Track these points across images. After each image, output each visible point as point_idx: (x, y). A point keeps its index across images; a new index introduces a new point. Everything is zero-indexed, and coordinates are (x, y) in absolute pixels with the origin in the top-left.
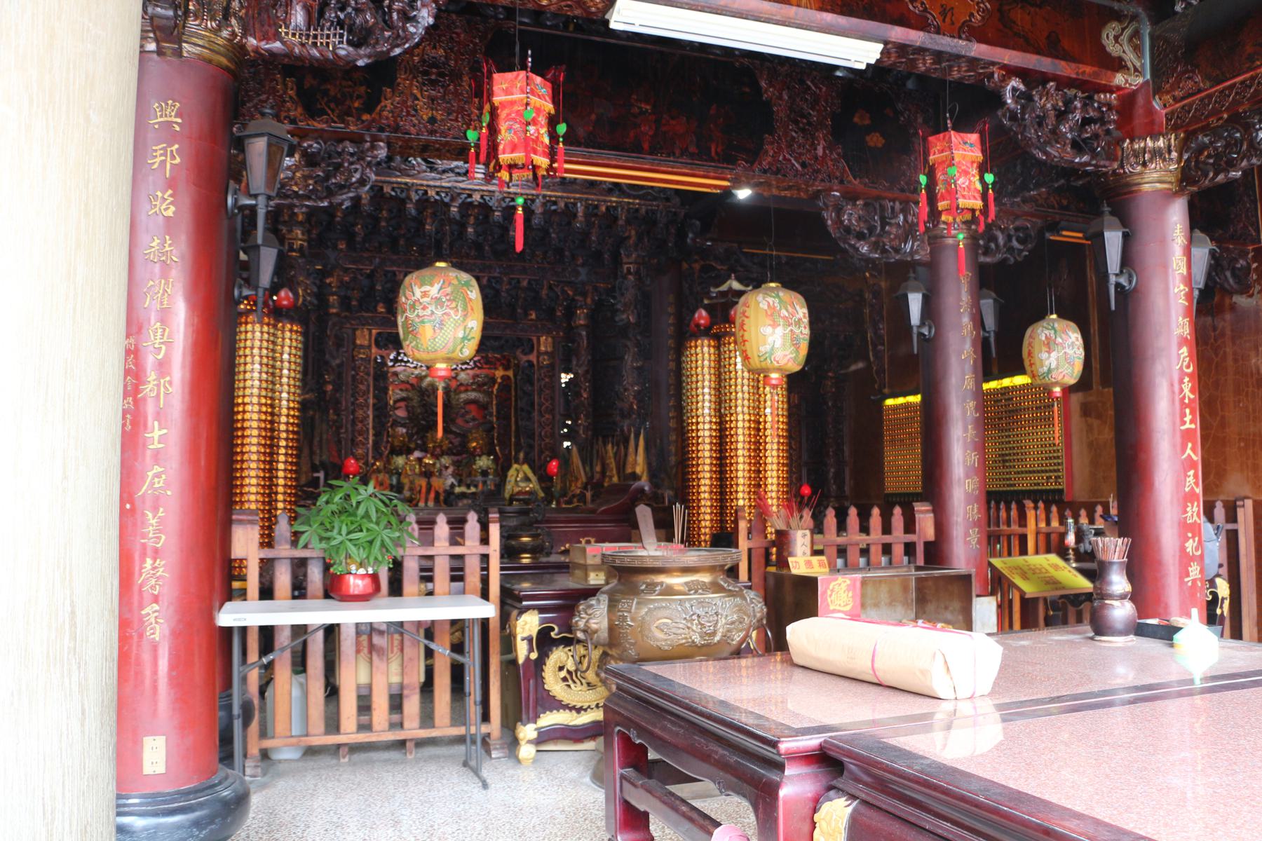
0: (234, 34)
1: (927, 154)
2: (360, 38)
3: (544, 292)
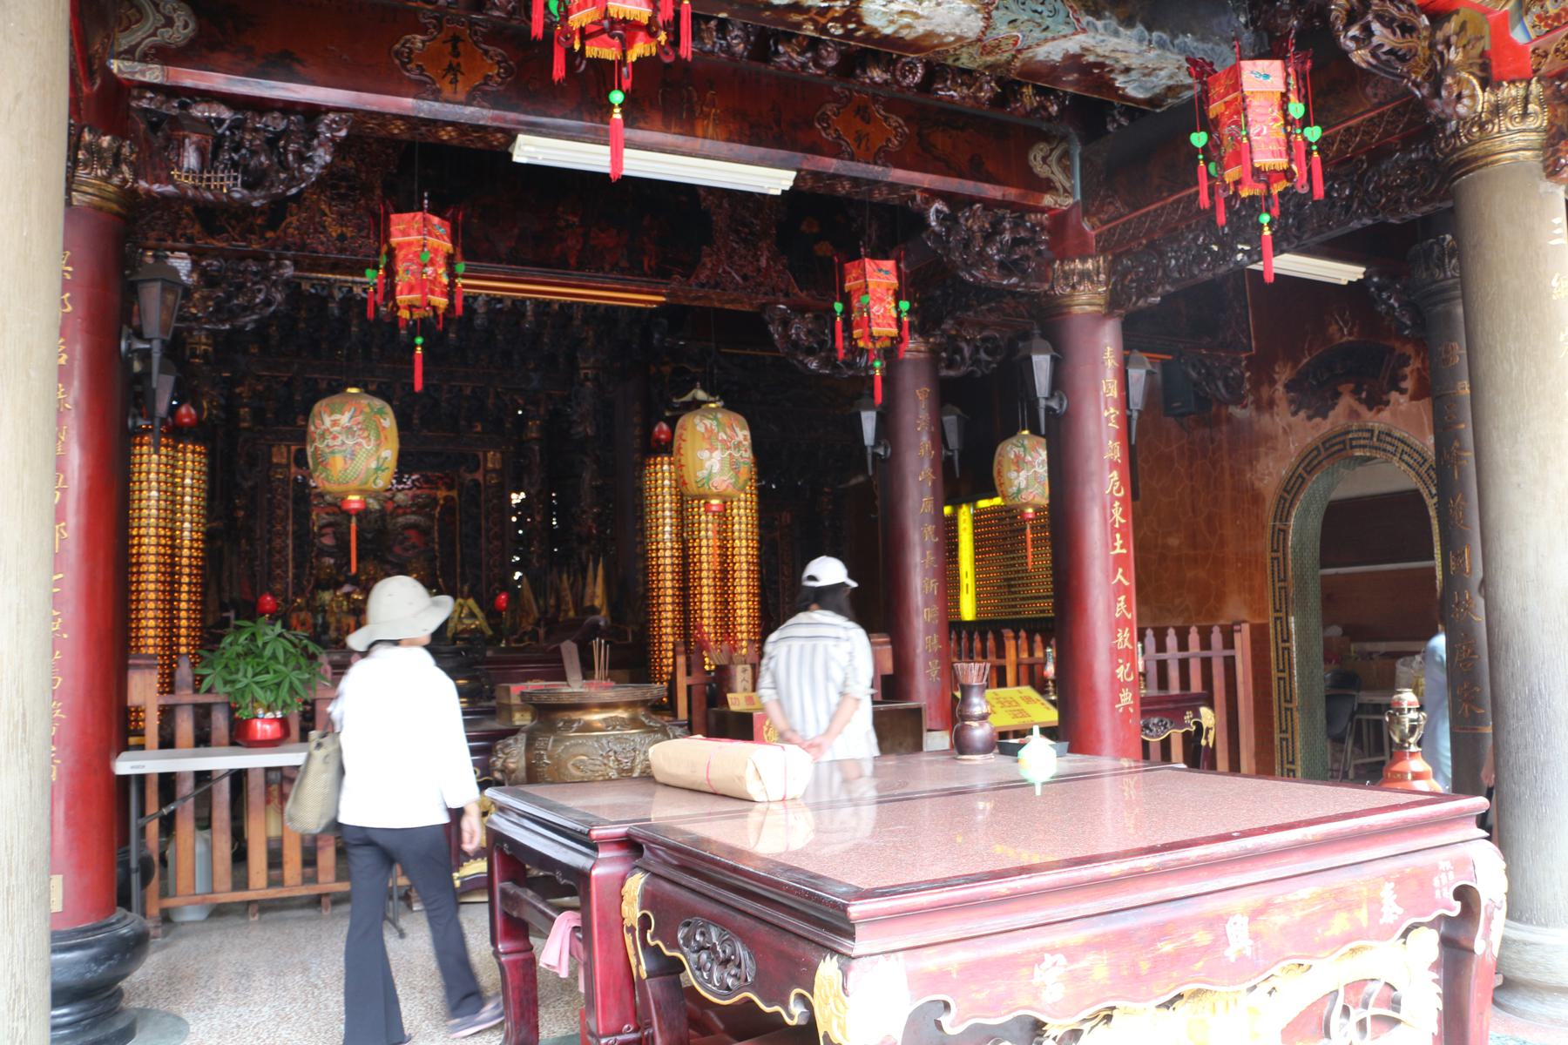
0: (125, 181)
1: (843, 281)
2: (254, 181)
3: (490, 402)
